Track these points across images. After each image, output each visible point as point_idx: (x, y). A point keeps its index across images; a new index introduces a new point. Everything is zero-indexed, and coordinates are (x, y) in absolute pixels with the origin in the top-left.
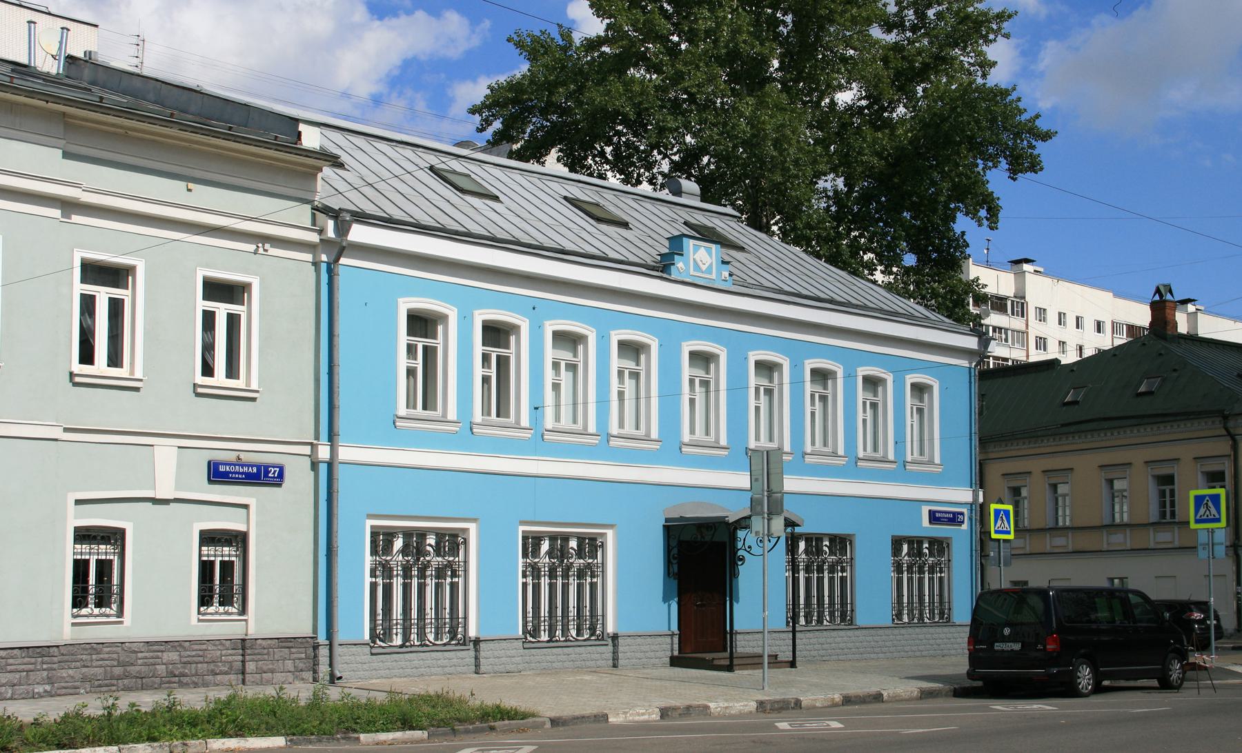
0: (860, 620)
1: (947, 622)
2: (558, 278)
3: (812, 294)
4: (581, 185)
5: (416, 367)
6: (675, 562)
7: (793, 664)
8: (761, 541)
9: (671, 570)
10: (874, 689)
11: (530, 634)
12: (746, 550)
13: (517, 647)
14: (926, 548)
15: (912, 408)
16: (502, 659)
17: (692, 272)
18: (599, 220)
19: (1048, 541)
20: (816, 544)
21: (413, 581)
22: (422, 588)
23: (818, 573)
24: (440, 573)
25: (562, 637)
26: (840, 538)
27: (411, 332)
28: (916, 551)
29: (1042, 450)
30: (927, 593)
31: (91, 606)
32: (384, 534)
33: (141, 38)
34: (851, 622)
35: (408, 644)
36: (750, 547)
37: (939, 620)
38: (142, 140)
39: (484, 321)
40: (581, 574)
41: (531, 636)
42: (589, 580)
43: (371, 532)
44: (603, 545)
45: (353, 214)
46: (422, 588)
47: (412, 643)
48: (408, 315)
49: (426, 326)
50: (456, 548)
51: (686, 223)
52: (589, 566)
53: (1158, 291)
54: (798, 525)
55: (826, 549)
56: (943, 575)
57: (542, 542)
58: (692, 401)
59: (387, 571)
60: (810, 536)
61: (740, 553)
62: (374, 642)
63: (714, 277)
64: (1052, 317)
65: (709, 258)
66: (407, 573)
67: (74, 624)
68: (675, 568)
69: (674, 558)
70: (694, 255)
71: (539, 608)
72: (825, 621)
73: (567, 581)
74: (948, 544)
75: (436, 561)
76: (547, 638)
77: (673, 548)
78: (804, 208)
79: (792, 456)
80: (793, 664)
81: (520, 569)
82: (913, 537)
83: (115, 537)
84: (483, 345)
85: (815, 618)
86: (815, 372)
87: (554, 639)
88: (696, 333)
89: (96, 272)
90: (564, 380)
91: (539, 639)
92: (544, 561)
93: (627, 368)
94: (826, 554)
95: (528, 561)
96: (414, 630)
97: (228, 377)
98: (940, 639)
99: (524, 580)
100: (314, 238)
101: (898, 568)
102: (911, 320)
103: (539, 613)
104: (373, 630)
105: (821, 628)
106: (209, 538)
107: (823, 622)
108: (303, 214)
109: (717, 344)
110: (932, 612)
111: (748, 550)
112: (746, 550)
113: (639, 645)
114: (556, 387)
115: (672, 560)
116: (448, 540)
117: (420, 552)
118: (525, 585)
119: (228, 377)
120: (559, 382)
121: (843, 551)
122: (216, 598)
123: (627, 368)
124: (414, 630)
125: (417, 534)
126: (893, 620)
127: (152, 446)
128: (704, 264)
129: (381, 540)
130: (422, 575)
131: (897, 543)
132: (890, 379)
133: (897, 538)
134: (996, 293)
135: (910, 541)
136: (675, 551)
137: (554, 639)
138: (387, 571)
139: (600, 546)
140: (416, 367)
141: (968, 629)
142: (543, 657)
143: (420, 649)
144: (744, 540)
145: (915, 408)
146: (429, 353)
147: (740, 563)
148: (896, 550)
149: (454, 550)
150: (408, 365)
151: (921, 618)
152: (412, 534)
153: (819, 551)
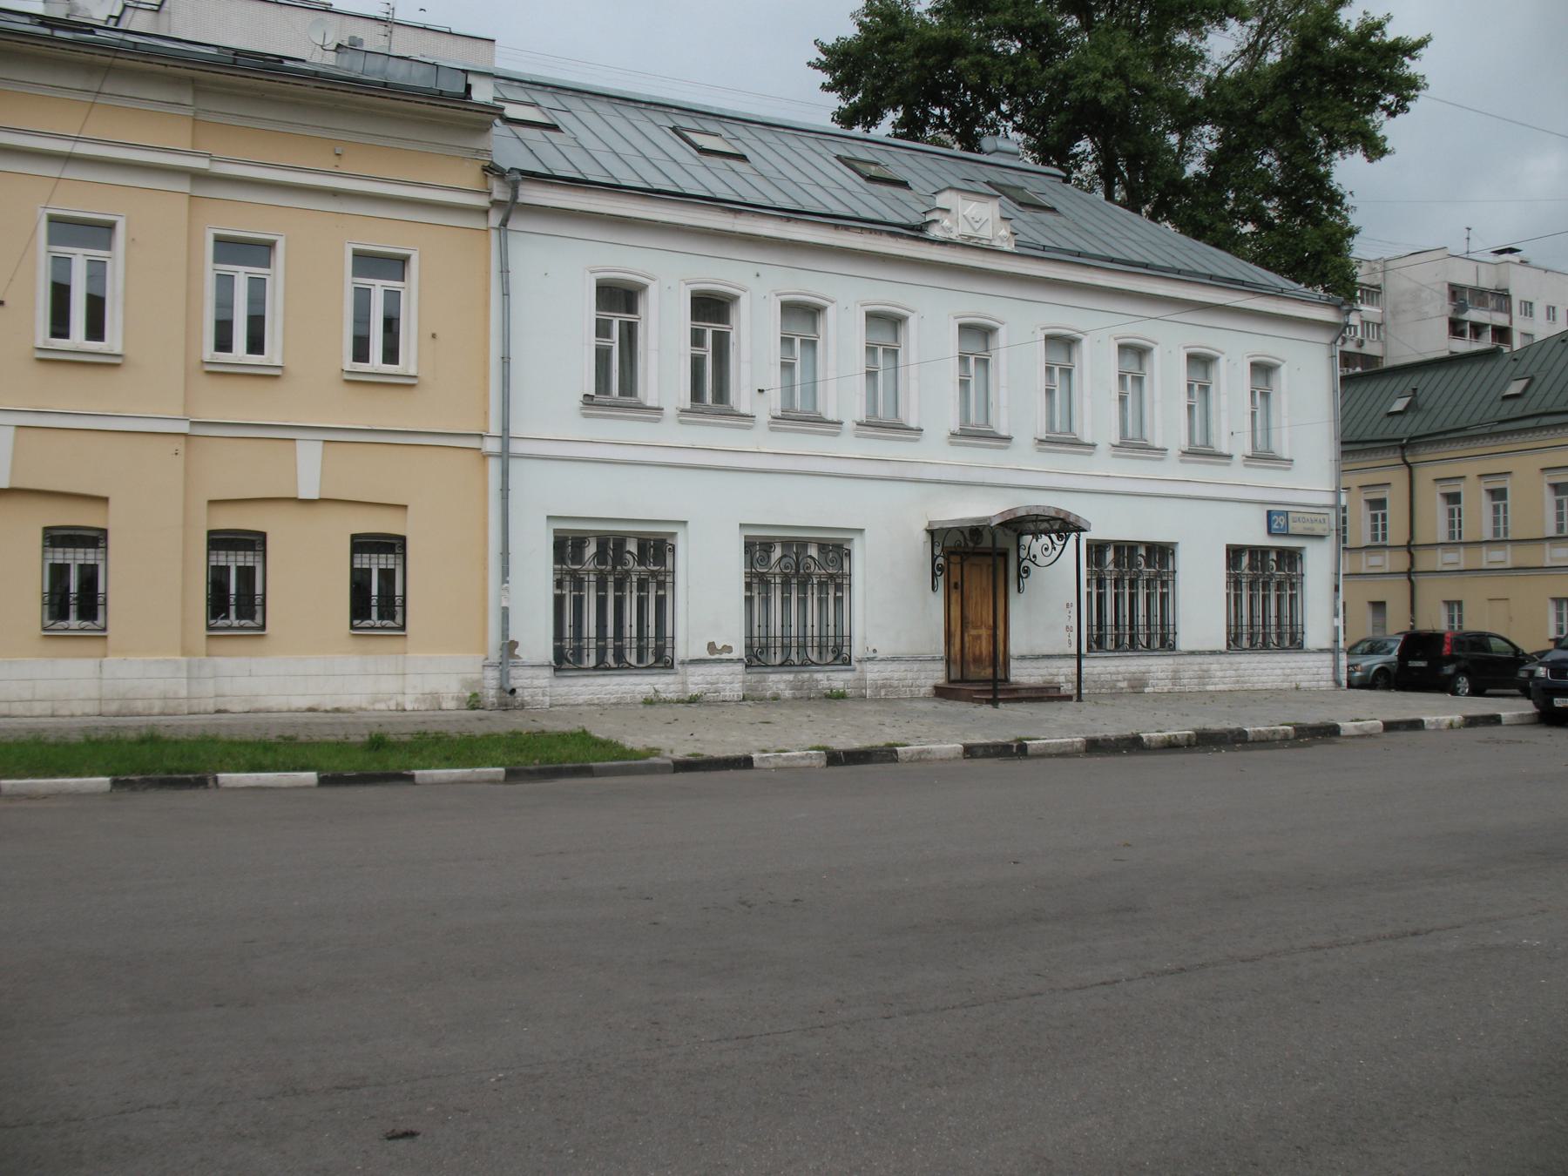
0: (1182, 645)
1: (1299, 649)
3: (1188, 268)
4: (868, 144)
5: (705, 355)
7: (1079, 699)
8: (1046, 549)
10: (1127, 730)
11: (756, 657)
12: (1030, 560)
13: (737, 672)
16: (608, 687)
18: (872, 179)
19: (1484, 555)
20: (1263, 558)
22: (1133, 597)
23: (1263, 590)
24: (1279, 586)
26: (1289, 551)
29: (1497, 449)
31: (233, 615)
32: (760, 544)
33: (392, 7)
34: (1172, 647)
35: (602, 666)
37: (656, 662)
38: (1295, 299)
39: (598, 281)
40: (1279, 586)
42: (1289, 592)
43: (745, 543)
45: (523, 172)
46: (1133, 597)
48: (598, 288)
49: (270, 250)
50: (839, 561)
51: (988, 183)
52: (831, 576)
53: (837, 39)
54: (1085, 531)
64: (1539, 310)
66: (601, 585)
67: (209, 636)
71: (605, 626)
72: (1272, 645)
74: (1301, 555)
77: (938, 557)
80: (1079, 699)
83: (254, 542)
85: (1260, 640)
89: (368, 263)
90: (799, 360)
91: (580, 666)
93: (880, 345)
96: (610, 652)
97: (385, 362)
98: (1285, 662)
100: (482, 202)
102: (1279, 295)
103: (1133, 623)
106: (361, 544)
108: (470, 176)
111: (1033, 560)
112: (1030, 560)
117: (619, 557)
119: (385, 362)
120: (704, 353)
121: (1164, 563)
122: (73, 609)
123: (880, 345)
124: (610, 652)
127: (295, 440)
128: (977, 222)
129: (567, 546)
130: (620, 586)
133: (1097, 543)
134: (1475, 285)
135: (1254, 551)
140: (705, 355)
142: (583, 689)
144: (1029, 548)
146: (629, 332)
147: (1024, 575)
150: (598, 343)
151: (619, 655)
153: (1265, 566)
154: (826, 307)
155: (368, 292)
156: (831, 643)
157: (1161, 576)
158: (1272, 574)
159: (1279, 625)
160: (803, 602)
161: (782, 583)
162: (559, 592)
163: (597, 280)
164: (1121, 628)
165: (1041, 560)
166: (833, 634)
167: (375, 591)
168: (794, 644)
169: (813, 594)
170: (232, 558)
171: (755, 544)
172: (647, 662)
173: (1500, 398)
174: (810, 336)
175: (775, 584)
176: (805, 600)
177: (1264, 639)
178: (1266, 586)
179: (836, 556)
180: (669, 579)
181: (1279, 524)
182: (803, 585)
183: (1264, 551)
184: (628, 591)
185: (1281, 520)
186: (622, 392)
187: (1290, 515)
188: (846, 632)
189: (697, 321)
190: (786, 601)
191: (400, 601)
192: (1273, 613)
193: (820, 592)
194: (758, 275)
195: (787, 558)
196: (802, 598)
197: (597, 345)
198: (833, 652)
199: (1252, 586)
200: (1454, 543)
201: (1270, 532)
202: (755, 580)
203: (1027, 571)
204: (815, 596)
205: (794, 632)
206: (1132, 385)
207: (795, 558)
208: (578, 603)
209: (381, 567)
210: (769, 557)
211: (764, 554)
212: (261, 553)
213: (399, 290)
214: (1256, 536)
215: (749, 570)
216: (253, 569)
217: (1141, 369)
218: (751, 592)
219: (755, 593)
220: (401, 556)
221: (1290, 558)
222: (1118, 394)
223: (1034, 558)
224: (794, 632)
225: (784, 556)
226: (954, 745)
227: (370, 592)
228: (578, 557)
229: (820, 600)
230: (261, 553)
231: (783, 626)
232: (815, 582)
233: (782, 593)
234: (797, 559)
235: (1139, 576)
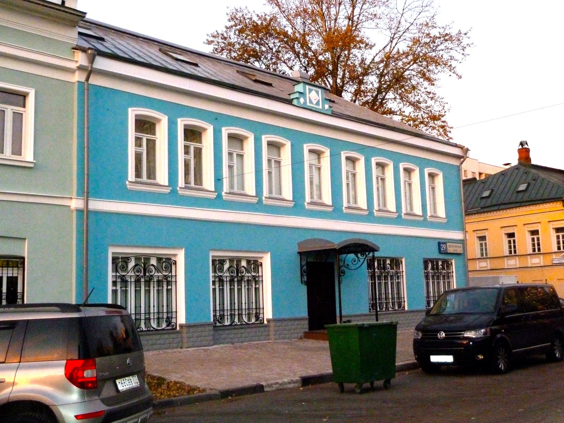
2: (228, 100)
3: (127, 56)
6: (305, 274)
9: (303, 279)
11: (218, 321)
14: (388, 264)
15: (405, 183)
17: (308, 104)
21: (129, 289)
22: (386, 284)
23: (385, 280)
24: (159, 282)
25: (239, 322)
27: (186, 138)
28: (435, 267)
30: (390, 292)
36: (348, 265)
41: (220, 322)
44: (175, 263)
47: (141, 329)
48: (136, 120)
50: (257, 267)
54: (376, 251)
55: (388, 266)
56: (399, 281)
57: (225, 263)
58: (270, 173)
59: (221, 281)
60: (380, 259)
61: (343, 268)
62: (216, 323)
63: (320, 107)
65: (317, 96)
68: (305, 278)
69: (305, 272)
70: (309, 94)
73: (137, 288)
75: (157, 275)
76: (229, 323)
77: (304, 266)
78: (254, 35)
79: (333, 208)
81: (211, 279)
82: (380, 257)
84: (136, 131)
85: (385, 306)
86: (231, 137)
87: (233, 324)
88: (408, 158)
90: (236, 163)
92: (131, 275)
94: (389, 269)
95: (216, 275)
99: (114, 288)
101: (427, 277)
104: (215, 316)
105: (389, 312)
107: (389, 309)
109: (192, 118)
110: (393, 304)
113: (279, 326)
114: (231, 167)
115: (341, 274)
116: (165, 262)
118: (214, 290)
125: (144, 258)
126: (370, 309)
131: (426, 262)
132: (288, 145)
135: (432, 261)
136: (305, 268)
137: (233, 324)
138: (221, 281)
139: (174, 263)
141: (307, 322)
143: (241, 326)
145: (430, 187)
147: (342, 274)
148: (426, 268)
149: (256, 269)
150: (136, 150)
152: (234, 260)
154: (161, 120)
155: (3, 113)
156: (165, 316)
157: (397, 274)
158: (389, 271)
159: (393, 298)
160: (148, 292)
161: (135, 281)
162: (114, 288)
163: (136, 116)
164: (374, 300)
165: (352, 266)
166: (134, 313)
167: (4, 290)
168: (143, 317)
169: (154, 287)
170: (5, 272)
171: (118, 258)
172: (162, 327)
173: (515, 192)
174: (277, 158)
175: (131, 282)
176: (149, 291)
177: (386, 306)
178: (386, 278)
179: (167, 264)
180: (174, 280)
181: (443, 248)
182: (148, 283)
183: (437, 260)
184: (129, 286)
185: (443, 246)
186: (149, 177)
187: (448, 244)
188: (174, 310)
189: (231, 148)
190: (137, 292)
191: (21, 296)
192: (383, 291)
193: (158, 286)
194: (216, 119)
195: (138, 266)
196: (123, 290)
197: (135, 151)
198: (166, 321)
199: (433, 279)
200: (484, 257)
201: (440, 252)
202: (119, 280)
203: (344, 272)
204: (156, 288)
205: (143, 311)
206: (237, 158)
207: (143, 265)
208: (222, 291)
209: (9, 275)
210: (127, 267)
211: (124, 264)
212: (22, 268)
213: (4, 109)
214: (435, 255)
215: (114, 274)
216: (16, 278)
217: (409, 180)
218: (116, 286)
219: (118, 287)
220: (22, 268)
221: (447, 264)
222: (309, 176)
223: (347, 266)
224: (143, 311)
225: (230, 267)
226: (509, 340)
227: (2, 291)
228: (125, 268)
229: (158, 291)
230: (22, 268)
231: (136, 307)
232: (155, 280)
233: (136, 287)
234: (145, 266)
235: (388, 274)
